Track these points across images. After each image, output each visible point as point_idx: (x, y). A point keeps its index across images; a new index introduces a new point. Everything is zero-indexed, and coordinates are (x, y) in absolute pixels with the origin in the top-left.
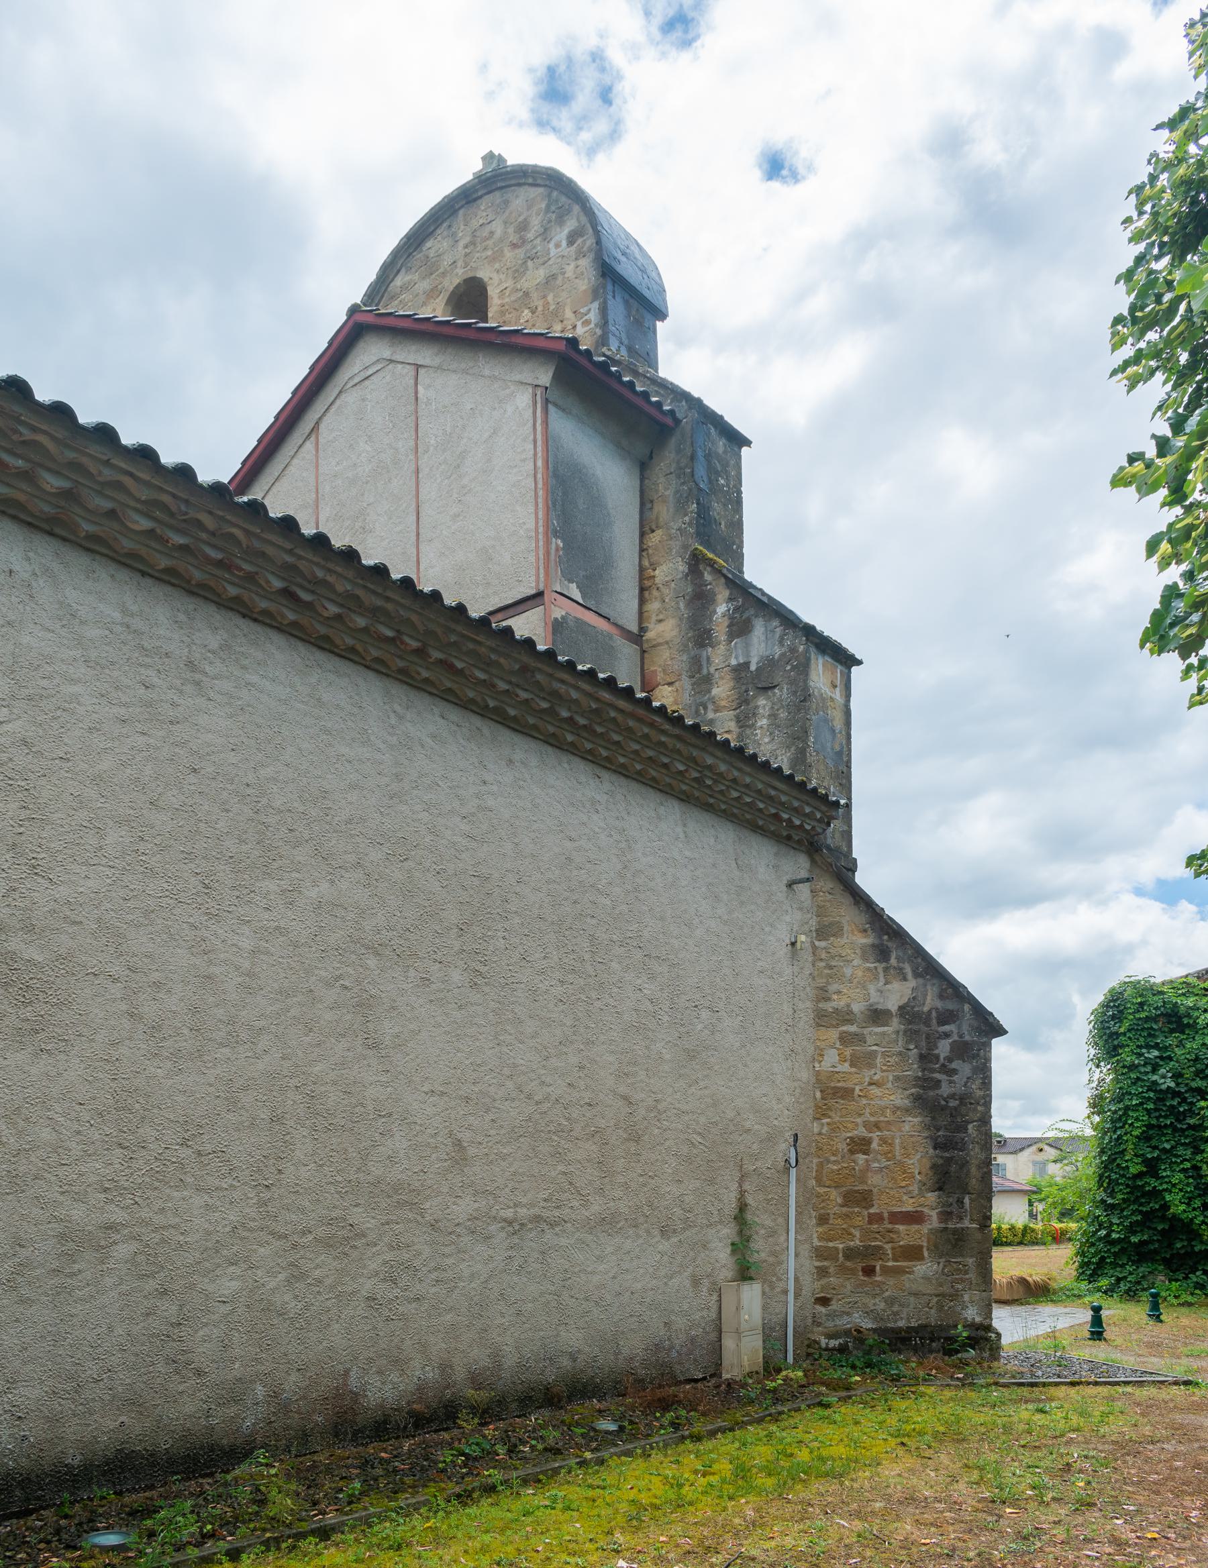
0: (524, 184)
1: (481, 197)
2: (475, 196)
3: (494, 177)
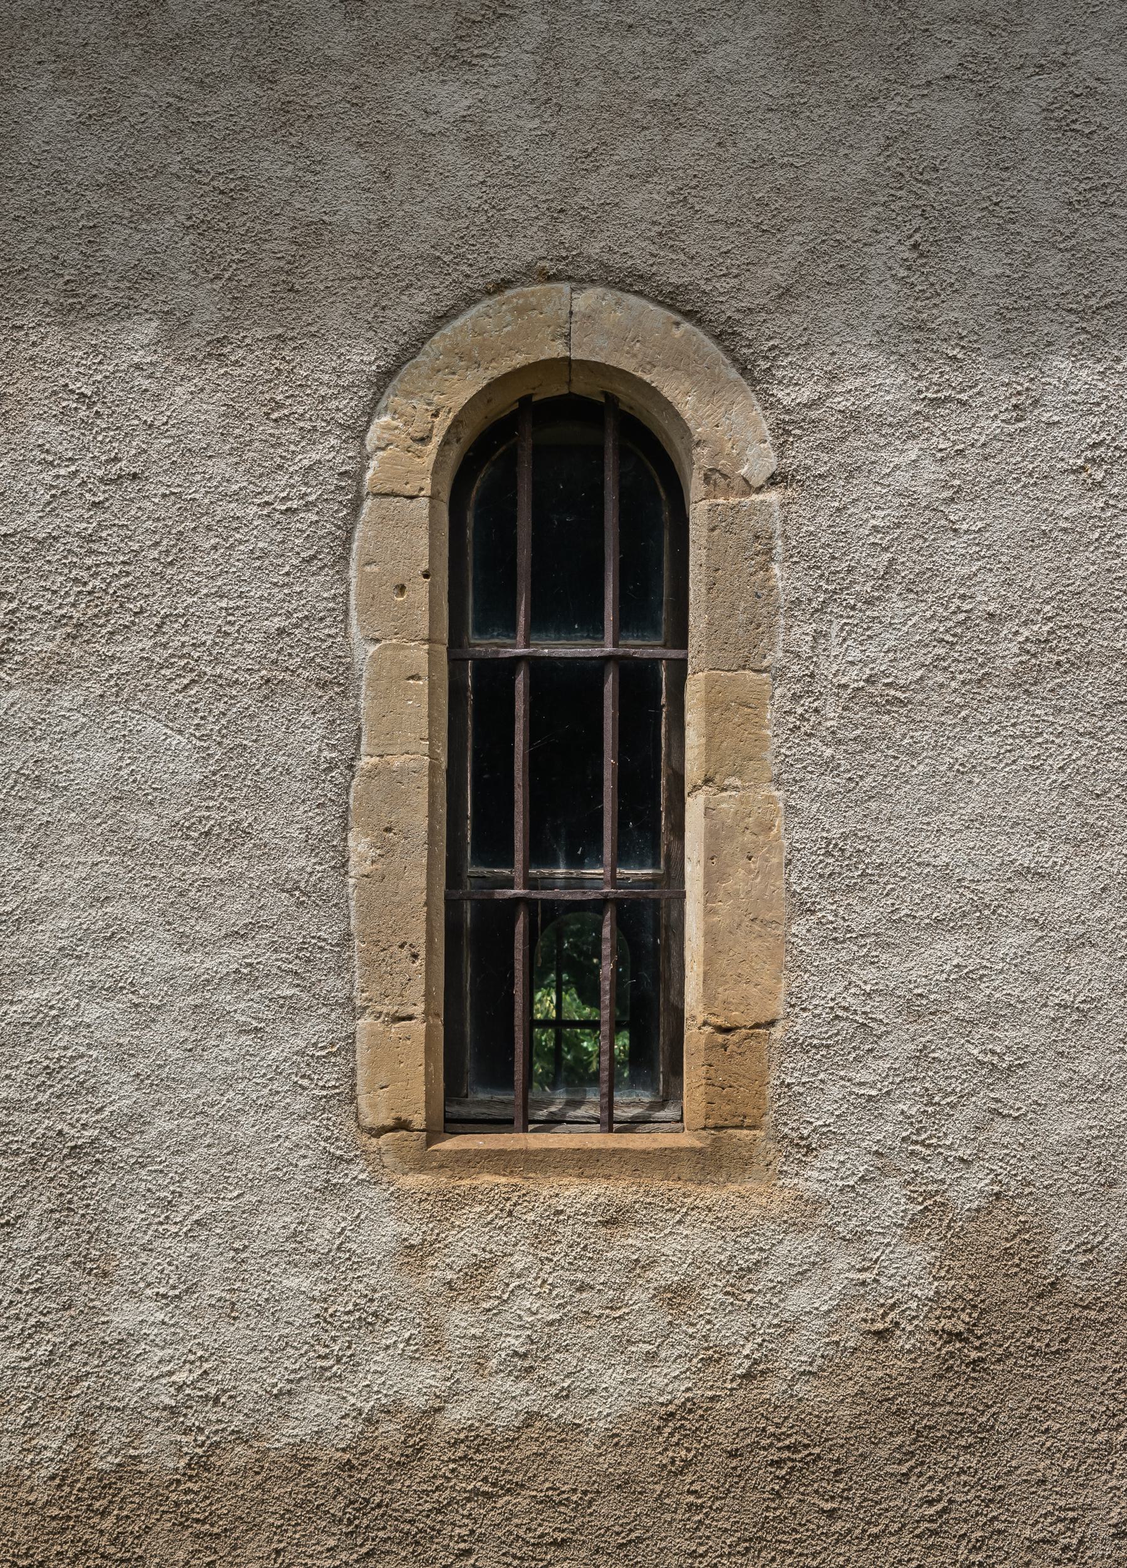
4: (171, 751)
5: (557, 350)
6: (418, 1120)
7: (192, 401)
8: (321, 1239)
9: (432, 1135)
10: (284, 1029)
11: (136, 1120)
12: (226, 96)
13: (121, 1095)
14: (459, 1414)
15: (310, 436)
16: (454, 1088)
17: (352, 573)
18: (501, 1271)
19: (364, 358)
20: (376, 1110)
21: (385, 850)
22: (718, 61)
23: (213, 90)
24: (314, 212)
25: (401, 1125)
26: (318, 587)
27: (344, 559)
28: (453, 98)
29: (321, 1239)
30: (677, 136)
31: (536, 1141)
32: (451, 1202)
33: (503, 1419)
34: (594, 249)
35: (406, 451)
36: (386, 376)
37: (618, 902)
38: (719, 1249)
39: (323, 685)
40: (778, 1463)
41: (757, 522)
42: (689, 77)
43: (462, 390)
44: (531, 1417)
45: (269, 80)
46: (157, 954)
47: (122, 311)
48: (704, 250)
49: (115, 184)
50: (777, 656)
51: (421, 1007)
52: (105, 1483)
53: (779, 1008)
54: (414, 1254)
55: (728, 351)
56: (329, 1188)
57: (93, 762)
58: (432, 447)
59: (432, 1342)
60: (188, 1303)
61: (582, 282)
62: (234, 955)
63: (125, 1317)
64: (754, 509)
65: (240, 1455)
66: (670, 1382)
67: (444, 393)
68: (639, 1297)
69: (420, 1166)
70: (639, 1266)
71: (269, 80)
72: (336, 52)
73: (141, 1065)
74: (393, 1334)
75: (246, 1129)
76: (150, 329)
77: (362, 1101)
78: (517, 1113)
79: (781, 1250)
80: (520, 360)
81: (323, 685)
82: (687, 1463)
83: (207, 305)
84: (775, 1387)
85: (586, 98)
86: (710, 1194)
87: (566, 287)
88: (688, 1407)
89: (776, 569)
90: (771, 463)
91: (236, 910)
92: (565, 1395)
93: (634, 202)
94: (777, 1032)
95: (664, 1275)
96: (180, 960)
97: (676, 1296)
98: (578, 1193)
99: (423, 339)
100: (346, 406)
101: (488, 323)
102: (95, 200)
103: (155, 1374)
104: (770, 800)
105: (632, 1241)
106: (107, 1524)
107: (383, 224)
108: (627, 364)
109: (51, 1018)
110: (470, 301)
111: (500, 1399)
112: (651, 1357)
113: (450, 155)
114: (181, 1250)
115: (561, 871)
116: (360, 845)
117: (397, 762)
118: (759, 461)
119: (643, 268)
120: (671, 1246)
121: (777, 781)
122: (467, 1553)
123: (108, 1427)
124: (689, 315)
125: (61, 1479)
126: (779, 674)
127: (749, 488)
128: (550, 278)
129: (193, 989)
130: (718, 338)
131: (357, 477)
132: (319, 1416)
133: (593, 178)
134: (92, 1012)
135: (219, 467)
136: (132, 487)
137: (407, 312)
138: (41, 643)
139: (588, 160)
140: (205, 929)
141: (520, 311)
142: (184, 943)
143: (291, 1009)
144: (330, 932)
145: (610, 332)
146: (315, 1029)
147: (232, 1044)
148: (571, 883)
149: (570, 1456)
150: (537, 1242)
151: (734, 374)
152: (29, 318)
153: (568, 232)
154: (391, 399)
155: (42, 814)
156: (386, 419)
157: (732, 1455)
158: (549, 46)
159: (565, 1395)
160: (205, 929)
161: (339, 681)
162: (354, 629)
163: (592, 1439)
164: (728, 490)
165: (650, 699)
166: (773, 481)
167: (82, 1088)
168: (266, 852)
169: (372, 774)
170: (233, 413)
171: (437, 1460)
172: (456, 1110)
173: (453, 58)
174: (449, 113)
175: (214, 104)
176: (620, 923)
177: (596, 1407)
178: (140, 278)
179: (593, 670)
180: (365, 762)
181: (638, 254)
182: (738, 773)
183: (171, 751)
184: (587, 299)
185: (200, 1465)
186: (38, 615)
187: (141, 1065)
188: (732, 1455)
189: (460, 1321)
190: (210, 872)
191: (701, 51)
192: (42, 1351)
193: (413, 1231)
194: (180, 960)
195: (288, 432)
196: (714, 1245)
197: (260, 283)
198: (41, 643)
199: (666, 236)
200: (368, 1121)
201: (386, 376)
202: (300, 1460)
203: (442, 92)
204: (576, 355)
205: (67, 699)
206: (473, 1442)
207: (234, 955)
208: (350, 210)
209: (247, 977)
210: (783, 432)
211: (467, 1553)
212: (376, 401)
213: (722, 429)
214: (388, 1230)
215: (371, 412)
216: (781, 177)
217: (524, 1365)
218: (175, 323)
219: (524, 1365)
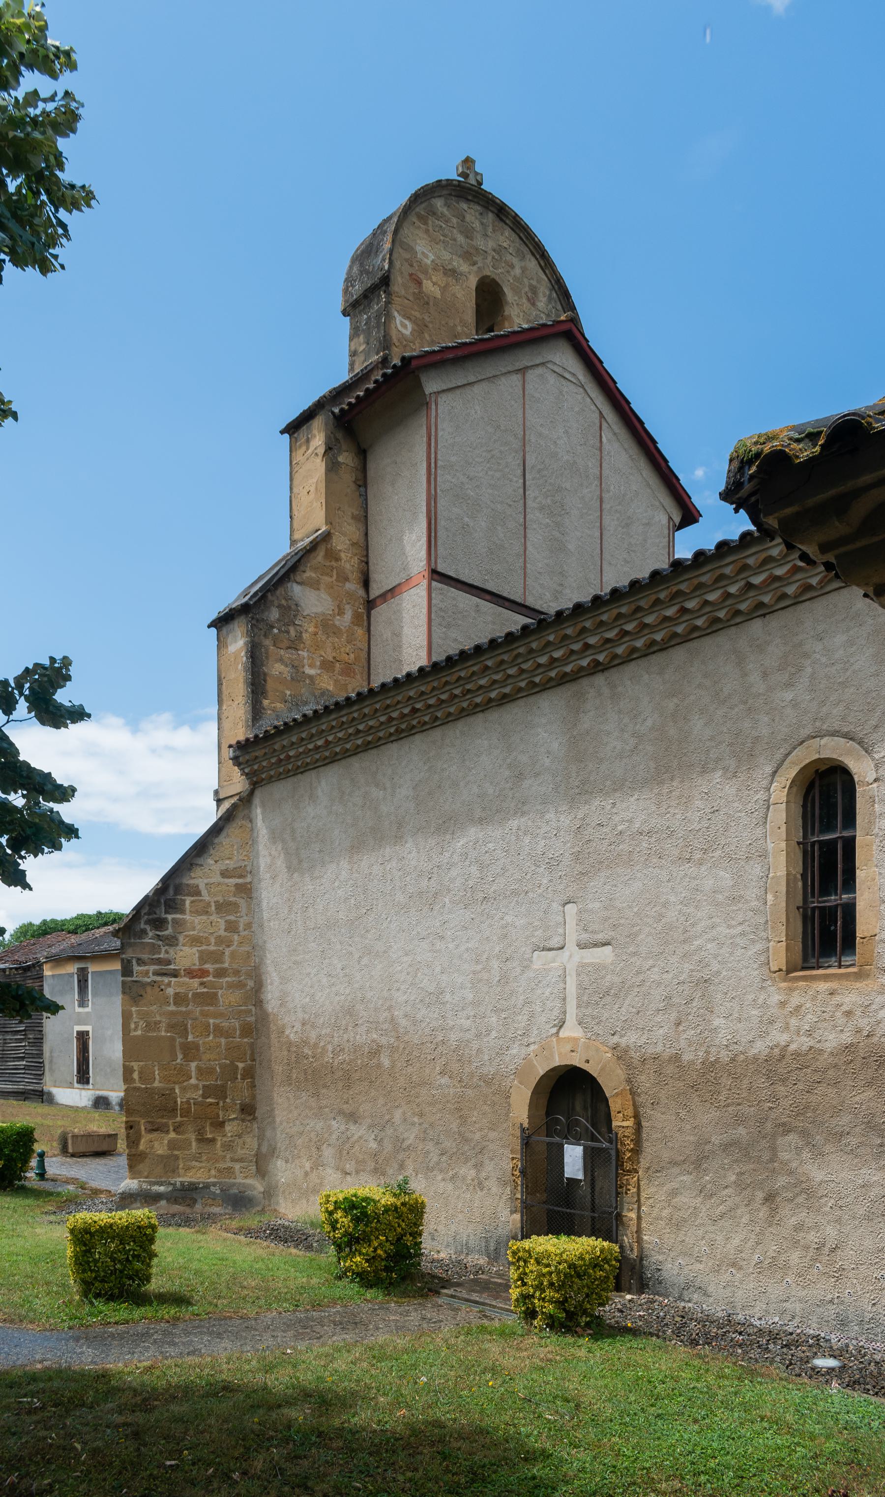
0: (537, 259)
1: (506, 224)
2: (504, 219)
3: (523, 227)
4: (726, 878)
5: (817, 756)
6: (784, 968)
7: (730, 789)
8: (760, 1001)
9: (788, 972)
10: (752, 947)
11: (718, 973)
12: (736, 710)
13: (715, 966)
14: (793, 1047)
15: (756, 792)
16: (805, 959)
17: (768, 826)
18: (803, 1008)
19: (769, 769)
20: (774, 968)
21: (776, 897)
22: (856, 667)
23: (733, 709)
24: (757, 734)
25: (780, 970)
26: (759, 831)
27: (766, 823)
28: (789, 695)
29: (760, 1001)
30: (846, 690)
31: (815, 972)
32: (791, 990)
33: (804, 1048)
34: (825, 727)
35: (780, 791)
36: (775, 772)
37: (841, 904)
38: (860, 1000)
39: (760, 856)
40: (876, 1061)
41: (871, 793)
42: (848, 673)
43: (793, 773)
44: (811, 1048)
45: (745, 703)
46: (723, 930)
47: (714, 770)
48: (854, 720)
49: (712, 738)
50: (876, 831)
51: (784, 939)
52: (713, 1064)
53: (877, 931)
54: (783, 1004)
55: (862, 747)
56: (762, 988)
57: (708, 884)
58: (786, 789)
59: (787, 1027)
60: (731, 1018)
61: (822, 737)
62: (739, 929)
63: (717, 1022)
64: (870, 790)
65: (742, 1057)
66: (847, 1038)
67: (790, 772)
68: (838, 1014)
69: (785, 981)
70: (839, 1006)
71: (745, 703)
72: (761, 691)
73: (719, 959)
74: (778, 1025)
75: (743, 974)
76: (720, 773)
77: (771, 964)
78: (815, 965)
79: (877, 1000)
80: (807, 761)
81: (760, 856)
82: (852, 1061)
83: (732, 763)
84: (875, 1039)
85: (822, 686)
86: (858, 985)
87: (818, 739)
88: (852, 1045)
89: (876, 806)
90: (874, 776)
91: (740, 918)
92: (819, 1041)
93: (835, 711)
94: (877, 938)
95: (845, 1008)
96: (728, 931)
97: (849, 1014)
98: (823, 986)
99: (783, 761)
100: (765, 783)
101: (800, 753)
102: (708, 744)
103: (722, 1037)
104: (875, 872)
105: (837, 999)
106: (713, 1074)
107: (773, 733)
108: (835, 756)
109: (700, 948)
110: (795, 748)
111: (803, 1043)
112: (842, 1031)
113: (789, 711)
114: (728, 1005)
115: (833, 898)
116: (770, 897)
117: (778, 874)
118: (871, 776)
119: (837, 729)
120: (847, 1000)
121: (877, 866)
122: (796, 1084)
123: (713, 1050)
124: (851, 739)
125: (703, 1063)
126: (877, 835)
127: (869, 784)
128: (814, 737)
129: (731, 938)
130: (859, 744)
131: (768, 801)
132: (760, 1048)
133: (824, 708)
134: (709, 946)
135: (736, 805)
136: (717, 813)
137: (778, 756)
138: (698, 856)
139: (823, 703)
140: (734, 923)
141: (807, 748)
142: (729, 927)
143: (753, 941)
144: (762, 921)
145: (831, 749)
146: (759, 946)
147: (740, 952)
148: (836, 900)
149: (821, 1058)
150: (813, 1000)
151: (864, 753)
152: (695, 776)
153: (818, 724)
154: (776, 778)
155: (698, 898)
156: (775, 784)
157: (864, 1058)
158: (813, 677)
159: (819, 1041)
160: (734, 923)
161: (764, 855)
162: (768, 840)
163: (826, 1054)
164: (863, 786)
165: (850, 845)
166: (875, 780)
167: (707, 965)
168: (747, 902)
169: (773, 878)
170: (739, 790)
171: (788, 1059)
172: (806, 965)
173: (789, 685)
174: (788, 700)
175: (733, 712)
176: (843, 912)
177: (828, 1045)
178: (718, 760)
179: (835, 841)
180: (771, 875)
181: (836, 726)
182: (866, 865)
183: (726, 878)
184: (824, 741)
185: (733, 1060)
186: (697, 849)
187: (719, 959)
188: (864, 1058)
189: (793, 1022)
190: (735, 908)
191: (853, 664)
192: (699, 1031)
193: (782, 998)
194: (728, 931)
195: (752, 792)
196: (858, 999)
197: (744, 754)
198: (698, 856)
199: (843, 719)
200: (773, 969)
201: (775, 772)
202: (755, 1059)
203: (786, 695)
204: (822, 757)
205: (703, 868)
206: (797, 1054)
207: (739, 929)
208: (765, 732)
209: (743, 934)
210: (877, 767)
211: (796, 1084)
212: (772, 780)
213: (862, 769)
214: (776, 998)
215: (771, 783)
216: (874, 694)
217: (809, 1033)
218: (726, 769)
219: (809, 1033)
